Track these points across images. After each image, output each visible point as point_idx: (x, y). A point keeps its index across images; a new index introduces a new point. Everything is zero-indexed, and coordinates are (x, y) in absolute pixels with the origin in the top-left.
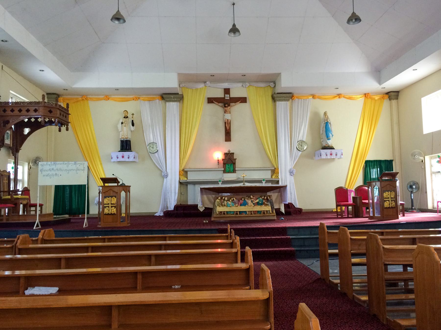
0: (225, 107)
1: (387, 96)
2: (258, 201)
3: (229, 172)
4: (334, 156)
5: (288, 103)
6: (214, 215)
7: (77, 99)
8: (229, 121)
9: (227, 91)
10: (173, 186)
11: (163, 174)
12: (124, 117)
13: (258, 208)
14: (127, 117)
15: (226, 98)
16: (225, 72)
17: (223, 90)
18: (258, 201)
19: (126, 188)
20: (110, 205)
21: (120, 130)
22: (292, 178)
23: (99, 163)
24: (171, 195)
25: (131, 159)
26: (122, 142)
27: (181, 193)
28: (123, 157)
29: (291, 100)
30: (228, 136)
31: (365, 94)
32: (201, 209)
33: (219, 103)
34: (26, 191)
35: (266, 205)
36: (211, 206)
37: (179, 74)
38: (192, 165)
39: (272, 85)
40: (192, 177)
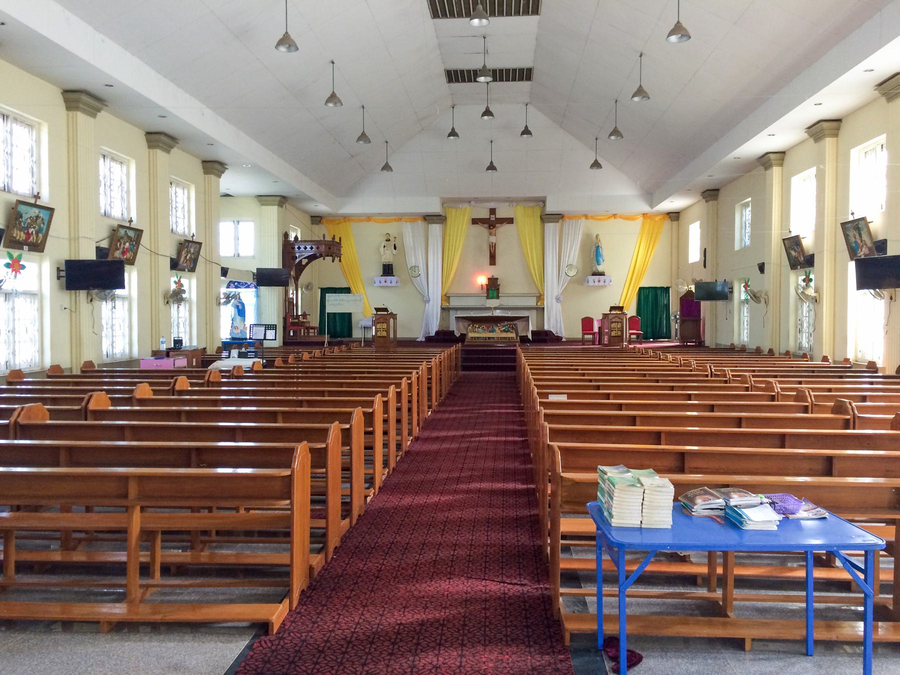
0: (490, 229)
1: (667, 217)
2: (504, 328)
3: (493, 298)
4: (602, 283)
5: (558, 225)
6: (467, 340)
7: (339, 220)
8: (494, 244)
9: (493, 211)
10: (435, 311)
11: (425, 299)
12: (387, 240)
13: (504, 335)
14: (389, 240)
15: (491, 219)
16: (490, 196)
17: (488, 211)
18: (504, 328)
19: (394, 316)
20: (382, 330)
21: (382, 254)
22: (559, 305)
23: (361, 286)
24: (433, 320)
25: (394, 284)
26: (384, 266)
27: (443, 319)
28: (386, 282)
29: (560, 221)
30: (493, 260)
31: (644, 214)
32: (457, 334)
33: (484, 224)
34: (304, 315)
35: (512, 332)
36: (465, 332)
37: (441, 198)
38: (454, 291)
39: (541, 204)
40: (454, 303)
